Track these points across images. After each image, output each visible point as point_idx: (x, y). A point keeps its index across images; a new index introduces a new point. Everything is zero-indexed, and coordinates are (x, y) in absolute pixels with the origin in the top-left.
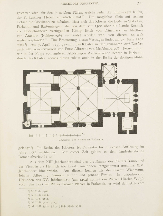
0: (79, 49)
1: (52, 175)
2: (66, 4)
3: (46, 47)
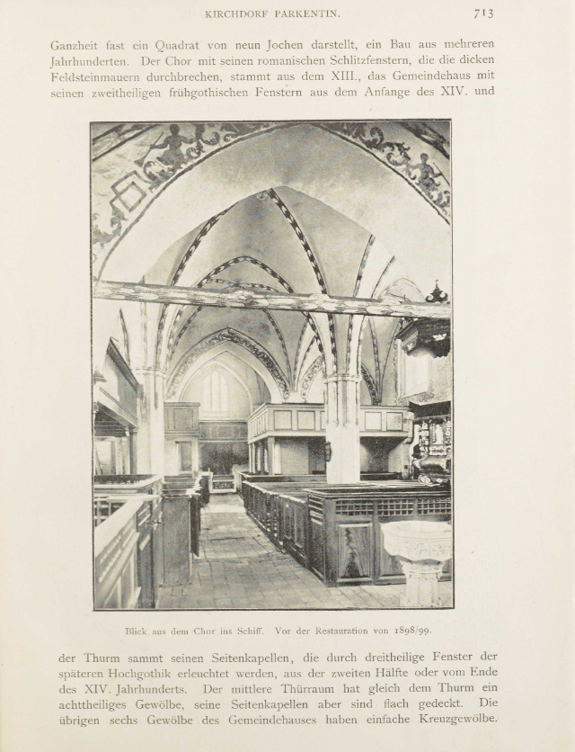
1: (380, 670)
2: (223, 15)
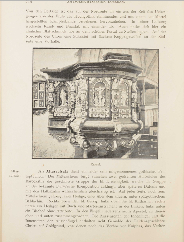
0: (66, 211)
1: (46, 205)
3: (121, 184)
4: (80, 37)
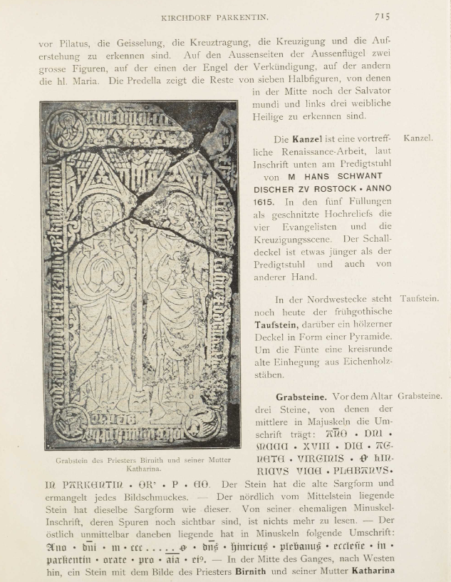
1: (328, 212)
2: (176, 19)
4: (353, 350)
